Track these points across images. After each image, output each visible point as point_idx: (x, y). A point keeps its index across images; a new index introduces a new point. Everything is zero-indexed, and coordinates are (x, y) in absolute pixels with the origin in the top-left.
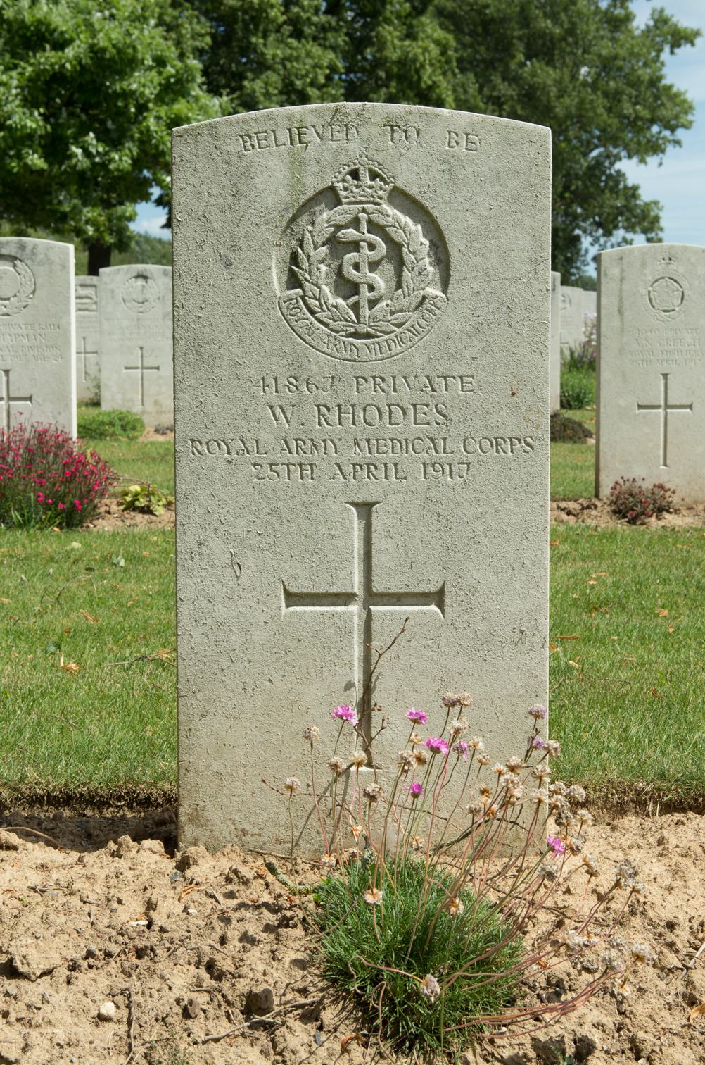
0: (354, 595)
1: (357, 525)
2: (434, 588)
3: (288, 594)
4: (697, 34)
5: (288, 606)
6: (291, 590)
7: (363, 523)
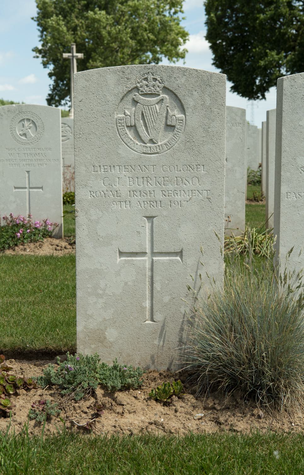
1: (27, 175)
2: (41, 186)
3: (14, 187)
4: (33, 50)
5: (120, 258)
6: (121, 251)
7: (150, 224)
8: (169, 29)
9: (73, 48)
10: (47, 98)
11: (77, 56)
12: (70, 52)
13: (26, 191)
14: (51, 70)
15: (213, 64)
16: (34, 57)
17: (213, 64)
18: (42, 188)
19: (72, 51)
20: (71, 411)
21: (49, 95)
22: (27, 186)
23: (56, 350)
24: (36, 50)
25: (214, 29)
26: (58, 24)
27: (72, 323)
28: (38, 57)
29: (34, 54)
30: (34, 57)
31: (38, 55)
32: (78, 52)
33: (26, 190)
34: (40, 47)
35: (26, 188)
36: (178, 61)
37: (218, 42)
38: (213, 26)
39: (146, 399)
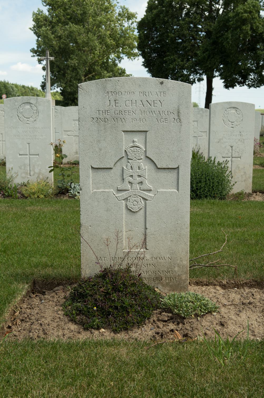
0: (27, 155)
8: (238, 9)
9: (47, 53)
10: (41, 85)
11: (50, 59)
12: (45, 56)
13: (27, 157)
14: (44, 65)
15: (143, 65)
16: (32, 56)
17: (143, 65)
18: (38, 155)
19: (46, 55)
20: (201, 294)
21: (43, 82)
22: (28, 154)
23: (102, 272)
24: (33, 51)
25: (142, 41)
26: (47, 34)
27: (78, 257)
28: (34, 56)
29: (32, 54)
30: (32, 56)
31: (34, 54)
32: (51, 55)
33: (28, 156)
34: (36, 49)
35: (27, 155)
36: (134, 59)
37: (181, 41)
38: (141, 40)
39: (153, 310)
